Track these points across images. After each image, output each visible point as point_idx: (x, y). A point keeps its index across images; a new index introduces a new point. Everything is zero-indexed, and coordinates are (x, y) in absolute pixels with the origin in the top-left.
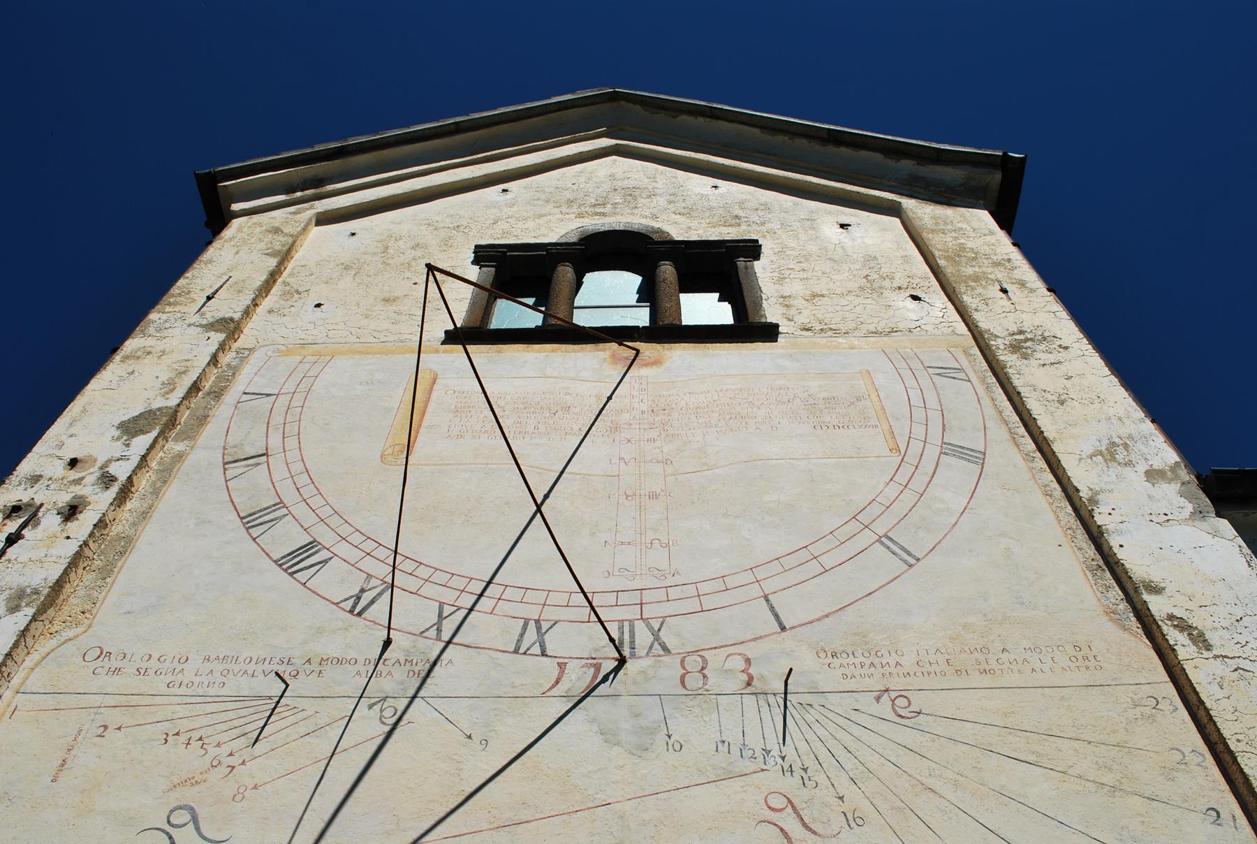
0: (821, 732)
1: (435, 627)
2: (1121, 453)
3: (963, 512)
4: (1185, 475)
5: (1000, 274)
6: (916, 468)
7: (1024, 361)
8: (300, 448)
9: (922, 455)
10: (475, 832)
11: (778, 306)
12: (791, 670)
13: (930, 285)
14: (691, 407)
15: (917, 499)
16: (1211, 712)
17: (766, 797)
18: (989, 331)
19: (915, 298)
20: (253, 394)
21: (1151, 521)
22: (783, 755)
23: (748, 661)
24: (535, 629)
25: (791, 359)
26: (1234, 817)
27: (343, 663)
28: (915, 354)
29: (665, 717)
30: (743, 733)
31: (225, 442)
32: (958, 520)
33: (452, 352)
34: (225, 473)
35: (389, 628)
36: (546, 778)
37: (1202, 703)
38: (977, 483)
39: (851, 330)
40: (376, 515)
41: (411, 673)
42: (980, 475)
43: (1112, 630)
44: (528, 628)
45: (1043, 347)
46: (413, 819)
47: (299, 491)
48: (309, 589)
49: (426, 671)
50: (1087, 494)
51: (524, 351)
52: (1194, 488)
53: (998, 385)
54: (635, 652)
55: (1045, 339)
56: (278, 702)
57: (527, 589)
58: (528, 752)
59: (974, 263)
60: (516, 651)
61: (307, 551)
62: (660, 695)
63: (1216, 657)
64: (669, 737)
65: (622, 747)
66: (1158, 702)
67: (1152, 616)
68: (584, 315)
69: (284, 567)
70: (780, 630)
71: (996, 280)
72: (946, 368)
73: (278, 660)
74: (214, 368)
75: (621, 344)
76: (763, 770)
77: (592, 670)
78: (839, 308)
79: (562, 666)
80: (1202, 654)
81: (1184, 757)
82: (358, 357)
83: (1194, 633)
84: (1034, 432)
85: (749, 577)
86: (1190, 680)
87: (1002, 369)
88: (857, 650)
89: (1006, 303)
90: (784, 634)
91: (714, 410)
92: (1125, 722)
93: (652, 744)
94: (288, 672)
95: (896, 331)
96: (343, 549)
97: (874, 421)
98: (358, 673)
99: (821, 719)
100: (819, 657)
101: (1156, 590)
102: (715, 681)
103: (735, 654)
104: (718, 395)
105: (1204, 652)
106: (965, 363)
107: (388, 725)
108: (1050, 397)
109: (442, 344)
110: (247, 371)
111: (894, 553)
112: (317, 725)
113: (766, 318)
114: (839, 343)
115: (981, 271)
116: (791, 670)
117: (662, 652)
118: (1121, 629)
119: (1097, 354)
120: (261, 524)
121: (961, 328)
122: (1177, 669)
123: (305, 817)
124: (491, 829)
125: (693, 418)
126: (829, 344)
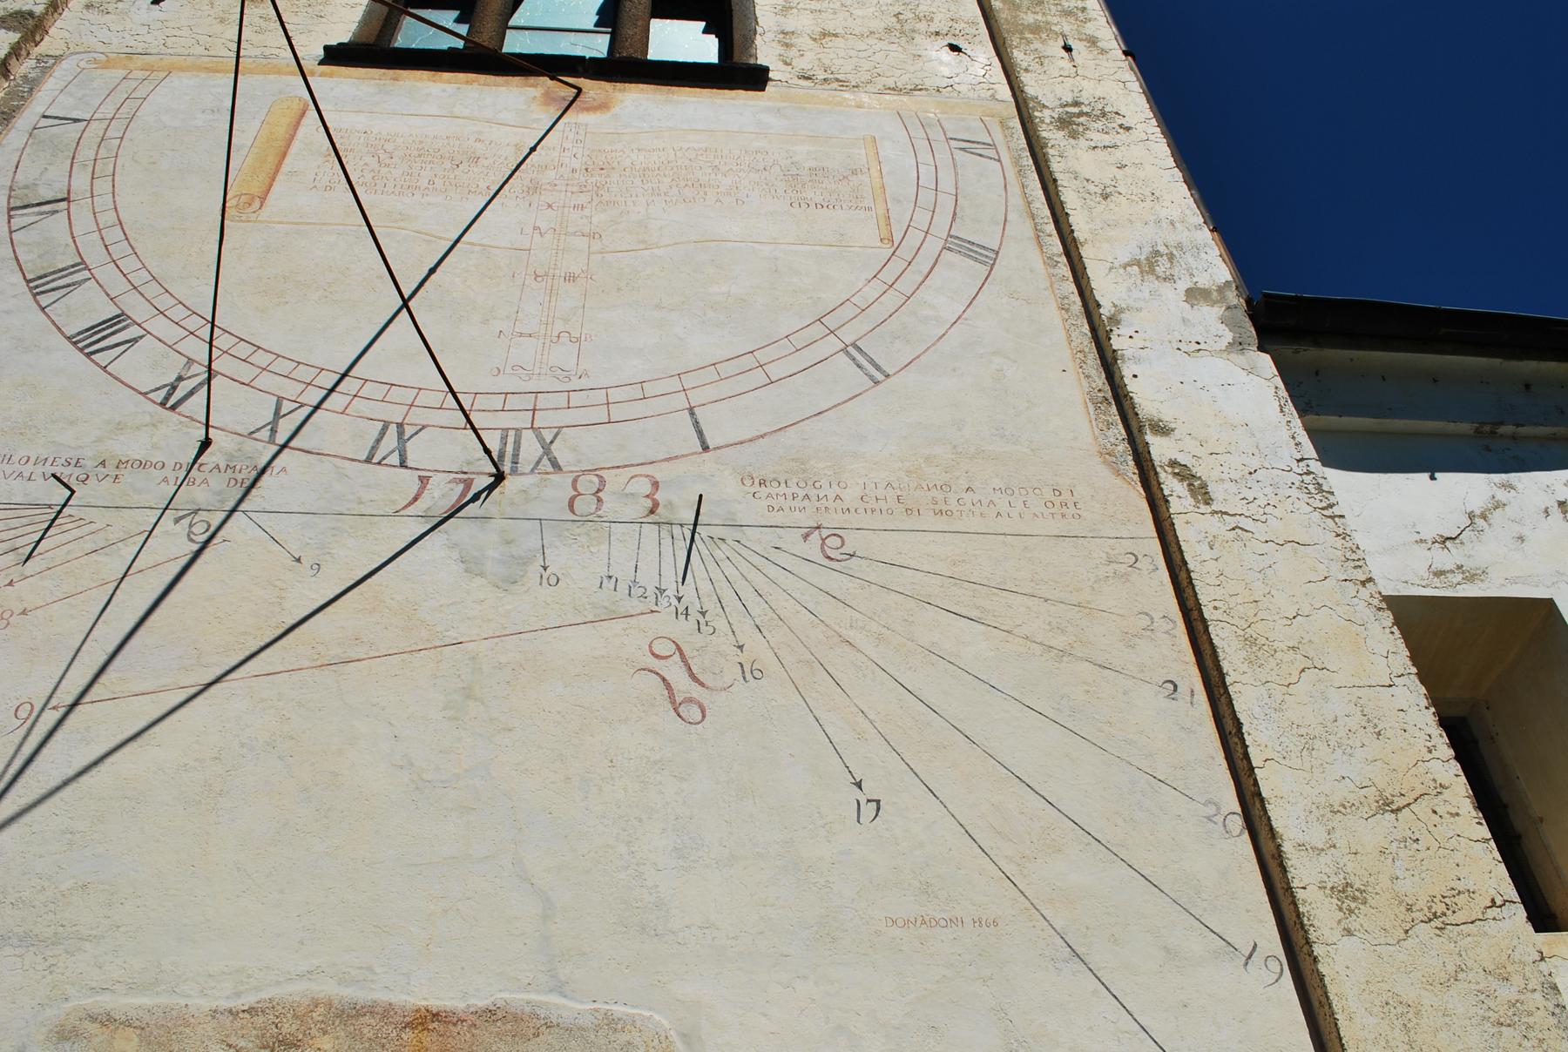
0: (730, 571)
1: (269, 427)
2: (1163, 265)
3: (955, 322)
4: (1233, 297)
5: (1067, 26)
6: (909, 265)
7: (1072, 141)
8: (113, 193)
9: (919, 249)
10: (293, 670)
11: (774, 44)
12: (701, 496)
13: (977, 32)
14: (637, 168)
15: (901, 303)
16: (1192, 574)
17: (651, 642)
18: (1037, 98)
19: (954, 48)
20: (56, 118)
21: (1179, 349)
22: (680, 596)
23: (656, 485)
24: (396, 434)
25: (778, 115)
26: (1192, 691)
27: (147, 467)
28: (938, 121)
29: (543, 546)
30: (636, 568)
31: (12, 181)
32: (947, 332)
33: (331, 75)
34: (9, 222)
35: (207, 426)
36: (388, 611)
37: (1185, 563)
38: (981, 288)
39: (863, 83)
40: (206, 284)
41: (233, 482)
42: (987, 279)
43: (1103, 473)
44: (387, 433)
45: (1099, 125)
46: (218, 653)
47: (107, 249)
48: (110, 374)
49: (252, 479)
50: (1109, 311)
51: (429, 80)
52: (1239, 314)
53: (1034, 168)
54: (517, 467)
55: (1104, 114)
56: (59, 512)
57: (392, 385)
58: (369, 580)
59: (1038, 9)
60: (368, 460)
61: (111, 326)
62: (540, 520)
63: (1214, 512)
64: (545, 569)
65: (486, 579)
66: (1137, 560)
67: (1151, 460)
68: (521, 39)
69: (80, 345)
70: (701, 450)
71: (1061, 34)
72: (973, 142)
73: (63, 461)
74: (3, 80)
75: (552, 79)
76: (652, 611)
77: (461, 487)
78: (853, 53)
79: (424, 480)
80: (1198, 508)
81: (1152, 623)
82: (203, 75)
83: (1195, 484)
84: (1064, 231)
85: (675, 384)
86: (1177, 537)
87: (1042, 148)
88: (792, 479)
89: (1066, 64)
90: (706, 455)
91: (667, 173)
92: (1092, 579)
93: (523, 576)
94: (74, 477)
95: (920, 90)
96: (159, 326)
97: (868, 202)
98: (165, 480)
99: (735, 558)
100: (744, 484)
101: (1162, 430)
102: (611, 506)
103: (641, 475)
104: (675, 154)
105: (1201, 506)
106: (999, 137)
107: (197, 543)
108: (1092, 188)
109: (319, 64)
110: (50, 85)
111: (859, 366)
112: (107, 540)
113: (757, 59)
114: (845, 98)
115: (1044, 19)
116: (701, 496)
117: (550, 469)
118: (1113, 474)
119: (1165, 140)
120: (53, 290)
121: (1005, 92)
122: (1167, 524)
123: (84, 648)
124: (313, 667)
125: (638, 181)
126: (831, 99)
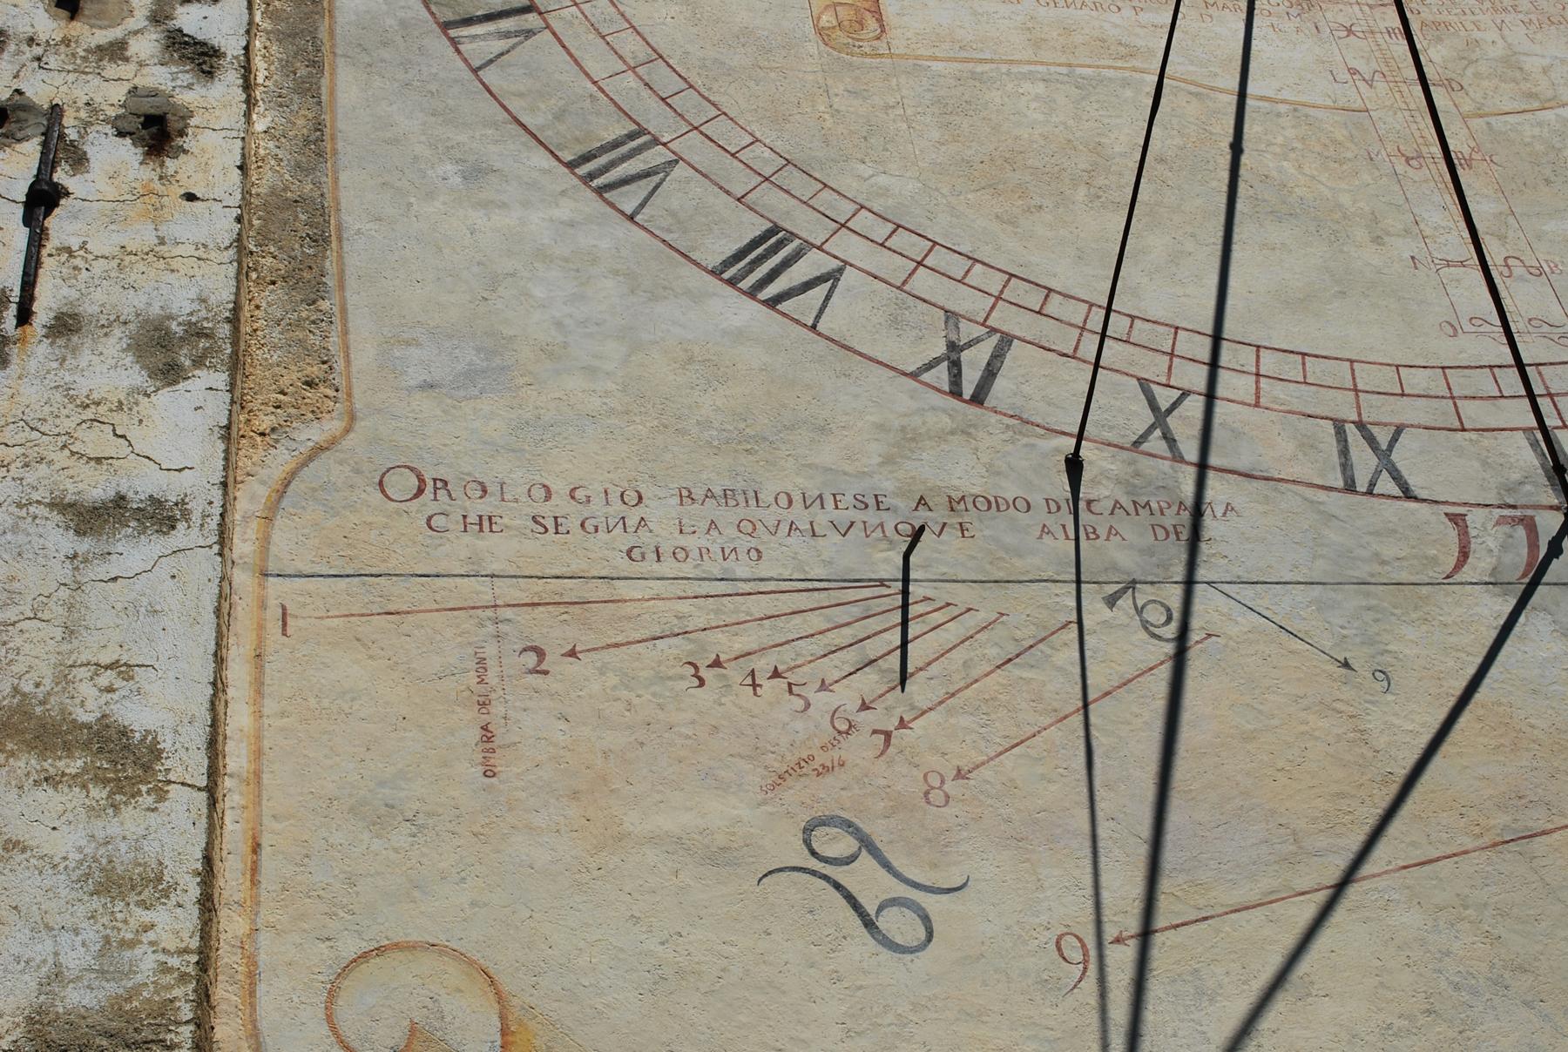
69: (746, 284)
